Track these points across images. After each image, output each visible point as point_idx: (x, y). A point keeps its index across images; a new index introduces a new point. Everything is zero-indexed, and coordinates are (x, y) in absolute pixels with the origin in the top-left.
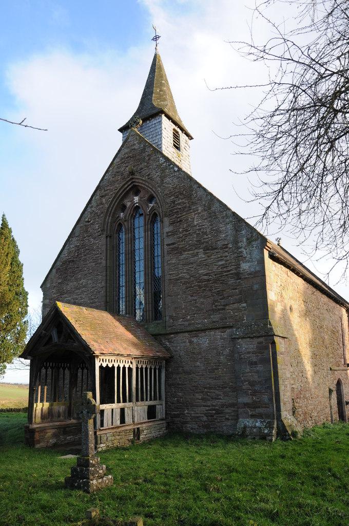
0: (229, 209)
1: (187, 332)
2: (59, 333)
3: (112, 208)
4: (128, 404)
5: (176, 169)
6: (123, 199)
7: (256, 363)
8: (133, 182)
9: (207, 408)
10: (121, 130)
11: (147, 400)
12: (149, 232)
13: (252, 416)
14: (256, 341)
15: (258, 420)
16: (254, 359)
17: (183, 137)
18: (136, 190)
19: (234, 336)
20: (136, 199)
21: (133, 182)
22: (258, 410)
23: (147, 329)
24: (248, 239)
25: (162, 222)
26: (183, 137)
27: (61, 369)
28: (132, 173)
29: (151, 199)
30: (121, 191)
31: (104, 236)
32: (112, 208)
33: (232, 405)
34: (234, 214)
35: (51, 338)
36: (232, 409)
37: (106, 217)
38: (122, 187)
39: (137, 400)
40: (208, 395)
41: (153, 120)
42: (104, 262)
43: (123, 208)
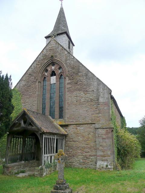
0: (95, 76)
1: (75, 124)
2: (25, 122)
3: (42, 70)
4: (53, 154)
5: (73, 57)
6: (47, 66)
7: (105, 139)
8: (52, 60)
9: (83, 157)
10: (46, 37)
11: (52, 153)
12: (41, 74)
13: (102, 160)
14: (105, 130)
15: (106, 162)
16: (104, 137)
17: (71, 45)
18: (53, 64)
19: (96, 127)
20: (53, 68)
21: (52, 60)
22: (106, 158)
23: (7, 115)
24: (103, 89)
25: (65, 78)
26: (71, 45)
27: (17, 138)
28: (52, 57)
29: (60, 68)
30: (47, 63)
31: (38, 82)
32: (42, 70)
33: (94, 156)
34: (97, 78)
35: (20, 124)
36: (95, 157)
37: (39, 74)
38: (47, 62)
39: (48, 154)
40: (83, 151)
41: (61, 35)
42: (37, 93)
43: (47, 71)
